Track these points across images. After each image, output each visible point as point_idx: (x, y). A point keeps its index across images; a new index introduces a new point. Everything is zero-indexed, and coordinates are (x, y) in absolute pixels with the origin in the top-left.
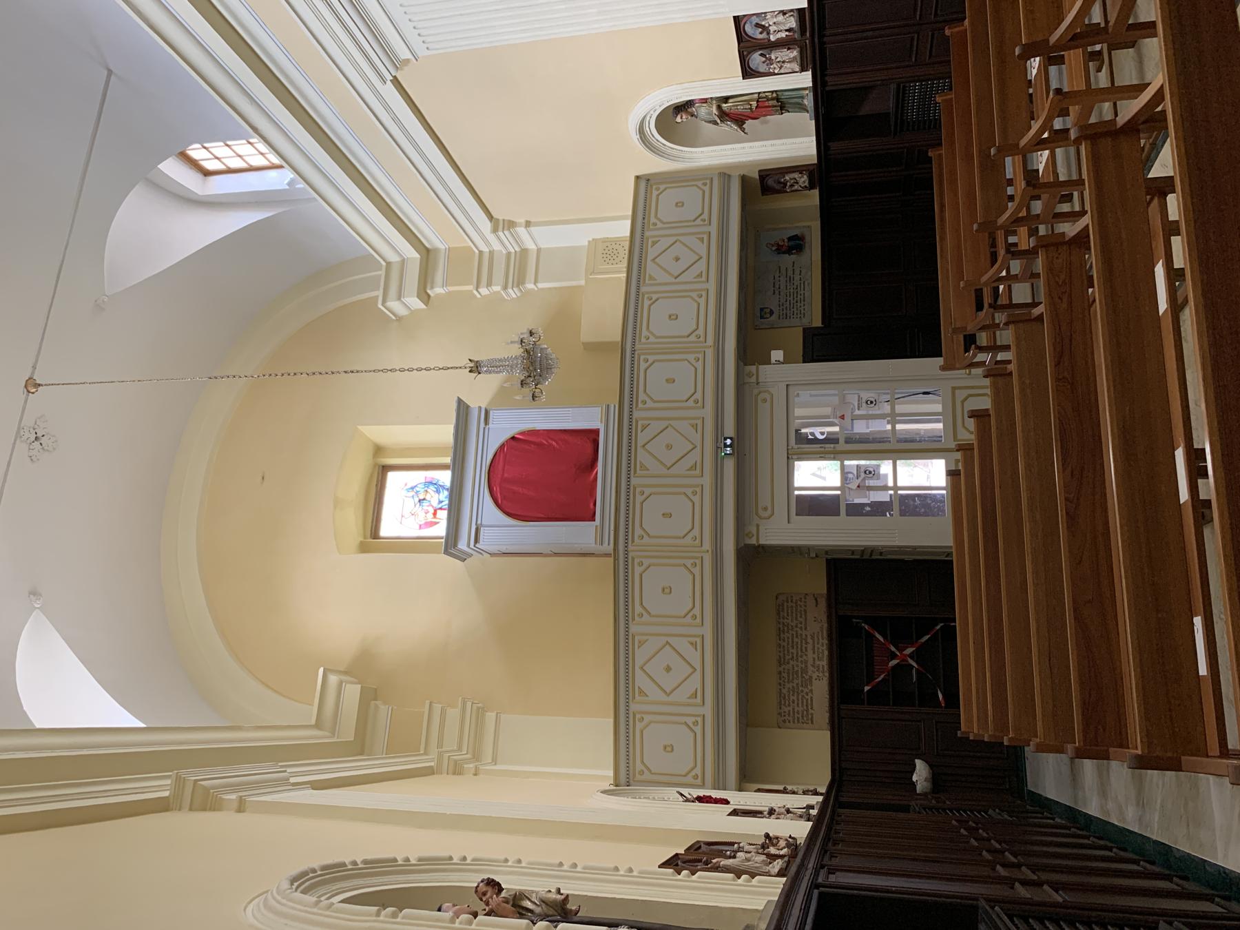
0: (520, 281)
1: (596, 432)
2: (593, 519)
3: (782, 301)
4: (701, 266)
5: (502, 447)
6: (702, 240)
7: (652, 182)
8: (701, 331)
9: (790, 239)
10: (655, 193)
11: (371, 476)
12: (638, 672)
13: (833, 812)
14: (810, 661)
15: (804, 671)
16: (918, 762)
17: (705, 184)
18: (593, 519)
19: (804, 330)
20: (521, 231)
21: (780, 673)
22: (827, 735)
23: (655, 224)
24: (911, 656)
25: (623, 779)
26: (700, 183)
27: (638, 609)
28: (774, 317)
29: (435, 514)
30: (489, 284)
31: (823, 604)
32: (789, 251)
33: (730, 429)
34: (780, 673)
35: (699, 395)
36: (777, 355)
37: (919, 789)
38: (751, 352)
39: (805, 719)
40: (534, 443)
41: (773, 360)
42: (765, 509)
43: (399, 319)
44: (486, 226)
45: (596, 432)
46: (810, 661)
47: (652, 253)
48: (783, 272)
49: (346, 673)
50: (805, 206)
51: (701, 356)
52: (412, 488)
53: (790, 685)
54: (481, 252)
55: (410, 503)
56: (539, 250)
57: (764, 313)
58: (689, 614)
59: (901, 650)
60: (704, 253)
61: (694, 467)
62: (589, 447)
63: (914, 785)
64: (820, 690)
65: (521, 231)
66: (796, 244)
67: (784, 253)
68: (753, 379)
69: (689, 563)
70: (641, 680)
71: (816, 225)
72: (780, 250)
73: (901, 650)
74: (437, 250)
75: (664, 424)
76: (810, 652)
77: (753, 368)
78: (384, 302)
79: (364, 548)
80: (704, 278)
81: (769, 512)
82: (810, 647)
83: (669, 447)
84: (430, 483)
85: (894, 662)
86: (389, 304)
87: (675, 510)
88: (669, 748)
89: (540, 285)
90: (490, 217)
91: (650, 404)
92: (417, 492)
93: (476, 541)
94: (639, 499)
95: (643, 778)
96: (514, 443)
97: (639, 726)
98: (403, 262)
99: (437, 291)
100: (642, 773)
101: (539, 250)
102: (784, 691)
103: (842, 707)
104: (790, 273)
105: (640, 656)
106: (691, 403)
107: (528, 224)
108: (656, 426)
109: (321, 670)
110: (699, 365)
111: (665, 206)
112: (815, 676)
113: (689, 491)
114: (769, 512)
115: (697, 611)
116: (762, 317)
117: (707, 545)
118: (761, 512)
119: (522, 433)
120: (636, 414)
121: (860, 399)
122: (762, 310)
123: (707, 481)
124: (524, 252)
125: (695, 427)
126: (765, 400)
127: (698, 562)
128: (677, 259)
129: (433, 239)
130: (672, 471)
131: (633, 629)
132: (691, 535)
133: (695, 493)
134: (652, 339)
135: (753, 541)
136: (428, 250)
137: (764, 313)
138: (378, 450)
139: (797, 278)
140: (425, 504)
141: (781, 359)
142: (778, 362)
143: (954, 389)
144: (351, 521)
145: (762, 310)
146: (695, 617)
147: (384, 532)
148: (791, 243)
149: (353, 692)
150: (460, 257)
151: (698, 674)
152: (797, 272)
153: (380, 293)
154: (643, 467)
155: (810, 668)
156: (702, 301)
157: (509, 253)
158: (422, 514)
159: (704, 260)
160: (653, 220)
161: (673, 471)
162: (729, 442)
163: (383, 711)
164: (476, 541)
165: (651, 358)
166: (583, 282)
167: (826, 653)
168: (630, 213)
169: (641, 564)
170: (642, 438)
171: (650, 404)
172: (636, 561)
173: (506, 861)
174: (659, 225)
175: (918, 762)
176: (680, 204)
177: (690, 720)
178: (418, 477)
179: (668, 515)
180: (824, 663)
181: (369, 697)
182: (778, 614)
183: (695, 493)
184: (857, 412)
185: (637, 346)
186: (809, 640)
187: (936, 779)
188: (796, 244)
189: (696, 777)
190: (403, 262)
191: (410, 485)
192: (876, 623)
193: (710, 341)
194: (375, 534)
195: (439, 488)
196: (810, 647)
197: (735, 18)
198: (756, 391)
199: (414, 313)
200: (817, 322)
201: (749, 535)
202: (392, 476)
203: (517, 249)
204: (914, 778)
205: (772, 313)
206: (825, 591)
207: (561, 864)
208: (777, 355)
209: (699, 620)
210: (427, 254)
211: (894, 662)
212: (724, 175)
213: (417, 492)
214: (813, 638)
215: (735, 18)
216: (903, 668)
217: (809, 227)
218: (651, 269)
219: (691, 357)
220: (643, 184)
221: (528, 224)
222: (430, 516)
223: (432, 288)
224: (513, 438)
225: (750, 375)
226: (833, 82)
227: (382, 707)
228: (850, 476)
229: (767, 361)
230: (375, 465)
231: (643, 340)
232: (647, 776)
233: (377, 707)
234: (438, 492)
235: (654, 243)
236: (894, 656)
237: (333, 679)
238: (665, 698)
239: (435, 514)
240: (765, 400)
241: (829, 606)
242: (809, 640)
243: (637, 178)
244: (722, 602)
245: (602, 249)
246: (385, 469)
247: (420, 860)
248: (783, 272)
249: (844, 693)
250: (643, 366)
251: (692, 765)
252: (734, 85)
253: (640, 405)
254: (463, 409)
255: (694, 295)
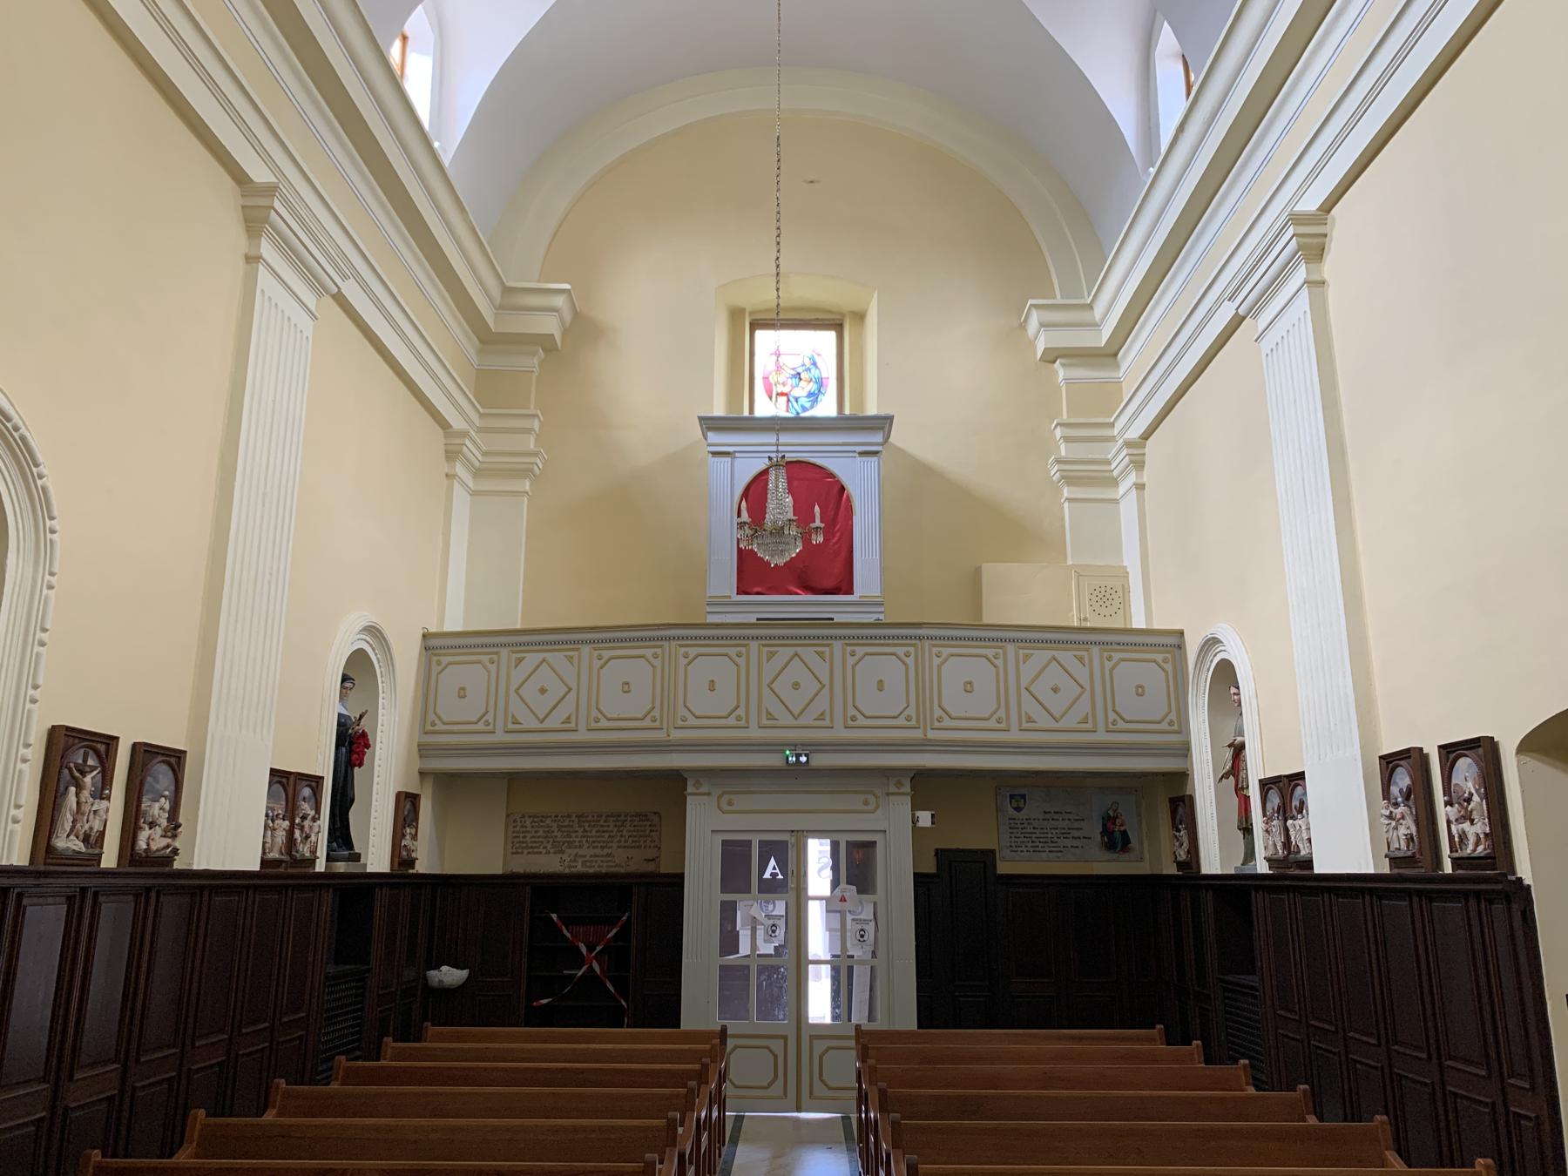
0: (1070, 480)
1: (850, 591)
2: (741, 591)
3: (1035, 823)
4: (1044, 721)
5: (832, 475)
6: (1085, 721)
7: (1177, 651)
8: (947, 723)
9: (1124, 833)
10: (1159, 657)
11: (829, 312)
12: (542, 655)
13: (328, 886)
14: (581, 852)
15: (571, 845)
16: (465, 973)
17: (1171, 723)
18: (741, 591)
19: (993, 852)
20: (1132, 478)
21: (569, 816)
22: (498, 870)
23: (1110, 659)
24: (591, 969)
25: (433, 642)
26: (1173, 716)
27: (606, 654)
28: (1011, 812)
29: (782, 394)
30: (1067, 439)
31: (650, 868)
32: (1106, 831)
33: (821, 760)
34: (569, 816)
35: (862, 721)
36: (925, 818)
37: (432, 973)
38: (927, 786)
39: (517, 844)
40: (836, 514)
41: (918, 814)
42: (730, 803)
43: (1023, 326)
44: (1134, 433)
45: (850, 591)
46: (581, 852)
47: (1066, 657)
48: (1076, 825)
49: (576, 313)
50: (1155, 857)
51: (913, 723)
52: (815, 364)
53: (555, 828)
54: (1112, 425)
55: (791, 363)
56: (1116, 501)
57: (1019, 800)
58: (613, 712)
59: (596, 958)
60: (1062, 725)
61: (770, 717)
62: (829, 583)
63: (437, 967)
64: (547, 863)
65: (1132, 478)
66: (1116, 841)
67: (1104, 825)
68: (893, 789)
69: (656, 713)
70: (532, 659)
71: (1143, 869)
72: (1109, 822)
73: (596, 958)
74: (1118, 366)
75: (826, 681)
76: (592, 851)
77: (907, 788)
78: (1036, 306)
79: (736, 314)
80: (1025, 725)
81: (725, 807)
82: (598, 851)
83: (796, 686)
84: (821, 383)
85: (584, 950)
86: (1034, 313)
87: (710, 702)
88: (462, 693)
89: (1066, 505)
90: (1146, 436)
91: (851, 661)
92: (809, 370)
93: (714, 454)
94: (732, 651)
95: (434, 665)
96: (836, 489)
97: (485, 659)
98: (1096, 325)
99: (1061, 371)
100: (439, 663)
101: (1116, 501)
102: (548, 821)
103: (528, 889)
104: (1075, 833)
105: (557, 658)
106: (852, 712)
107: (1140, 487)
108: (822, 670)
109: (567, 286)
110: (901, 721)
111: (1130, 672)
112: (565, 857)
113: (741, 712)
114: (725, 807)
115: (604, 723)
116: (1012, 797)
117: (676, 735)
118: (726, 797)
119: (849, 500)
120: (837, 645)
121: (866, 921)
122: (1023, 797)
123: (754, 733)
124: (1114, 482)
125: (821, 717)
126: (866, 803)
127: (657, 724)
128: (1055, 690)
129: (1133, 357)
130: (766, 691)
131: (586, 649)
132: (688, 715)
133: (739, 719)
134: (937, 661)
135: (690, 789)
136: (1116, 355)
137: (1019, 800)
138: (860, 317)
139: (1068, 842)
140: (795, 381)
141: (920, 824)
142: (915, 821)
143: (785, 1038)
144: (762, 296)
145: (1023, 797)
146: (597, 721)
147: (760, 335)
148: (1117, 834)
149: (549, 325)
150: (1109, 398)
151: (536, 725)
152: (1076, 843)
153: (1059, 300)
154: (771, 655)
155: (573, 852)
156: (992, 724)
157: (1109, 463)
158: (781, 379)
159: (1054, 725)
160: (1117, 656)
161: (766, 691)
162: (803, 759)
163: (533, 362)
164: (714, 454)
165: (910, 661)
166: (1070, 562)
167: (591, 871)
168: (1156, 627)
169: (655, 656)
170: (808, 653)
171: (851, 661)
172: (659, 651)
173: (52, 574)
174: (1108, 665)
175: (465, 973)
176: (1140, 691)
177: (489, 717)
178: (829, 369)
179: (712, 686)
180: (579, 868)
181: (545, 342)
182: (637, 815)
183: (739, 719)
184: (849, 917)
185: (926, 643)
186: (606, 851)
187: (445, 992)
188: (1116, 841)
189: (433, 724)
190: (1096, 325)
191: (817, 359)
192: (624, 934)
193: (931, 735)
194: (756, 325)
195: (814, 397)
196: (598, 851)
197: (1303, 773)
198: (878, 792)
199: (1032, 344)
200: (1003, 868)
201: (698, 784)
202: (831, 335)
203: (1115, 473)
204: (445, 968)
205: (1018, 809)
206: (663, 871)
207: (44, 630)
208: (925, 818)
209: (593, 725)
210: (1109, 355)
211: (584, 950)
212: (1185, 750)
213: (809, 370)
214: (608, 855)
215: (1303, 773)
216: (579, 960)
217: (1142, 859)
218: (1041, 656)
219: (912, 711)
220: (1173, 640)
221: (1140, 487)
222: (780, 389)
223: (1063, 365)
224: (843, 489)
225: (899, 784)
226: (1259, 901)
227: (536, 361)
228: (771, 907)
229: (915, 807)
230: (843, 315)
231: (935, 650)
232: (435, 669)
233: (535, 353)
234: (810, 394)
235: (1081, 659)
236: (591, 949)
237: (559, 301)
238: (513, 687)
239: (782, 394)
240: (866, 803)
241: (641, 875)
242: (606, 851)
243: (1181, 633)
244: (612, 753)
245: (1112, 590)
246: (838, 327)
247: (44, 489)
248: (1076, 825)
249: (547, 891)
250: (901, 651)
251: (445, 719)
252: (1257, 768)
253: (849, 649)
254: (882, 423)
255: (1001, 713)
